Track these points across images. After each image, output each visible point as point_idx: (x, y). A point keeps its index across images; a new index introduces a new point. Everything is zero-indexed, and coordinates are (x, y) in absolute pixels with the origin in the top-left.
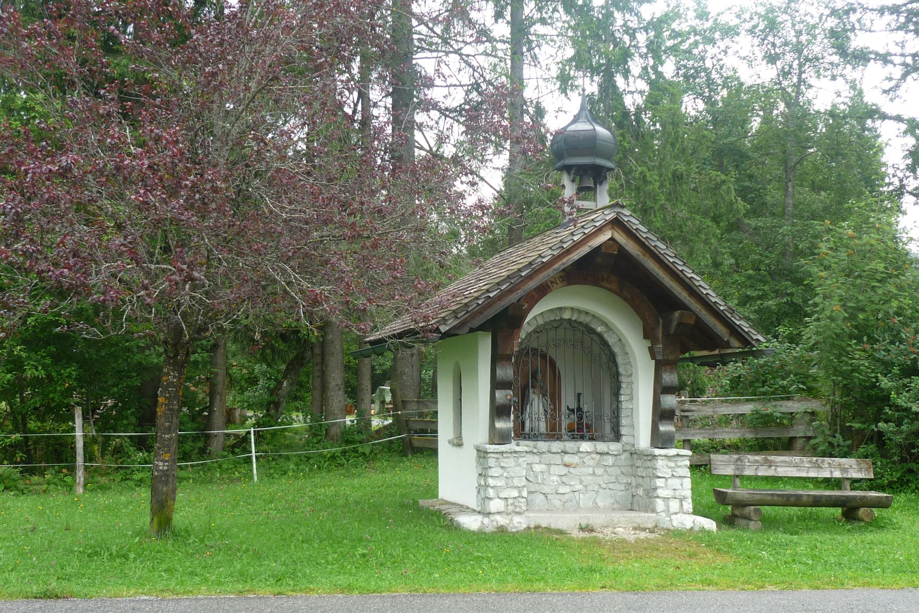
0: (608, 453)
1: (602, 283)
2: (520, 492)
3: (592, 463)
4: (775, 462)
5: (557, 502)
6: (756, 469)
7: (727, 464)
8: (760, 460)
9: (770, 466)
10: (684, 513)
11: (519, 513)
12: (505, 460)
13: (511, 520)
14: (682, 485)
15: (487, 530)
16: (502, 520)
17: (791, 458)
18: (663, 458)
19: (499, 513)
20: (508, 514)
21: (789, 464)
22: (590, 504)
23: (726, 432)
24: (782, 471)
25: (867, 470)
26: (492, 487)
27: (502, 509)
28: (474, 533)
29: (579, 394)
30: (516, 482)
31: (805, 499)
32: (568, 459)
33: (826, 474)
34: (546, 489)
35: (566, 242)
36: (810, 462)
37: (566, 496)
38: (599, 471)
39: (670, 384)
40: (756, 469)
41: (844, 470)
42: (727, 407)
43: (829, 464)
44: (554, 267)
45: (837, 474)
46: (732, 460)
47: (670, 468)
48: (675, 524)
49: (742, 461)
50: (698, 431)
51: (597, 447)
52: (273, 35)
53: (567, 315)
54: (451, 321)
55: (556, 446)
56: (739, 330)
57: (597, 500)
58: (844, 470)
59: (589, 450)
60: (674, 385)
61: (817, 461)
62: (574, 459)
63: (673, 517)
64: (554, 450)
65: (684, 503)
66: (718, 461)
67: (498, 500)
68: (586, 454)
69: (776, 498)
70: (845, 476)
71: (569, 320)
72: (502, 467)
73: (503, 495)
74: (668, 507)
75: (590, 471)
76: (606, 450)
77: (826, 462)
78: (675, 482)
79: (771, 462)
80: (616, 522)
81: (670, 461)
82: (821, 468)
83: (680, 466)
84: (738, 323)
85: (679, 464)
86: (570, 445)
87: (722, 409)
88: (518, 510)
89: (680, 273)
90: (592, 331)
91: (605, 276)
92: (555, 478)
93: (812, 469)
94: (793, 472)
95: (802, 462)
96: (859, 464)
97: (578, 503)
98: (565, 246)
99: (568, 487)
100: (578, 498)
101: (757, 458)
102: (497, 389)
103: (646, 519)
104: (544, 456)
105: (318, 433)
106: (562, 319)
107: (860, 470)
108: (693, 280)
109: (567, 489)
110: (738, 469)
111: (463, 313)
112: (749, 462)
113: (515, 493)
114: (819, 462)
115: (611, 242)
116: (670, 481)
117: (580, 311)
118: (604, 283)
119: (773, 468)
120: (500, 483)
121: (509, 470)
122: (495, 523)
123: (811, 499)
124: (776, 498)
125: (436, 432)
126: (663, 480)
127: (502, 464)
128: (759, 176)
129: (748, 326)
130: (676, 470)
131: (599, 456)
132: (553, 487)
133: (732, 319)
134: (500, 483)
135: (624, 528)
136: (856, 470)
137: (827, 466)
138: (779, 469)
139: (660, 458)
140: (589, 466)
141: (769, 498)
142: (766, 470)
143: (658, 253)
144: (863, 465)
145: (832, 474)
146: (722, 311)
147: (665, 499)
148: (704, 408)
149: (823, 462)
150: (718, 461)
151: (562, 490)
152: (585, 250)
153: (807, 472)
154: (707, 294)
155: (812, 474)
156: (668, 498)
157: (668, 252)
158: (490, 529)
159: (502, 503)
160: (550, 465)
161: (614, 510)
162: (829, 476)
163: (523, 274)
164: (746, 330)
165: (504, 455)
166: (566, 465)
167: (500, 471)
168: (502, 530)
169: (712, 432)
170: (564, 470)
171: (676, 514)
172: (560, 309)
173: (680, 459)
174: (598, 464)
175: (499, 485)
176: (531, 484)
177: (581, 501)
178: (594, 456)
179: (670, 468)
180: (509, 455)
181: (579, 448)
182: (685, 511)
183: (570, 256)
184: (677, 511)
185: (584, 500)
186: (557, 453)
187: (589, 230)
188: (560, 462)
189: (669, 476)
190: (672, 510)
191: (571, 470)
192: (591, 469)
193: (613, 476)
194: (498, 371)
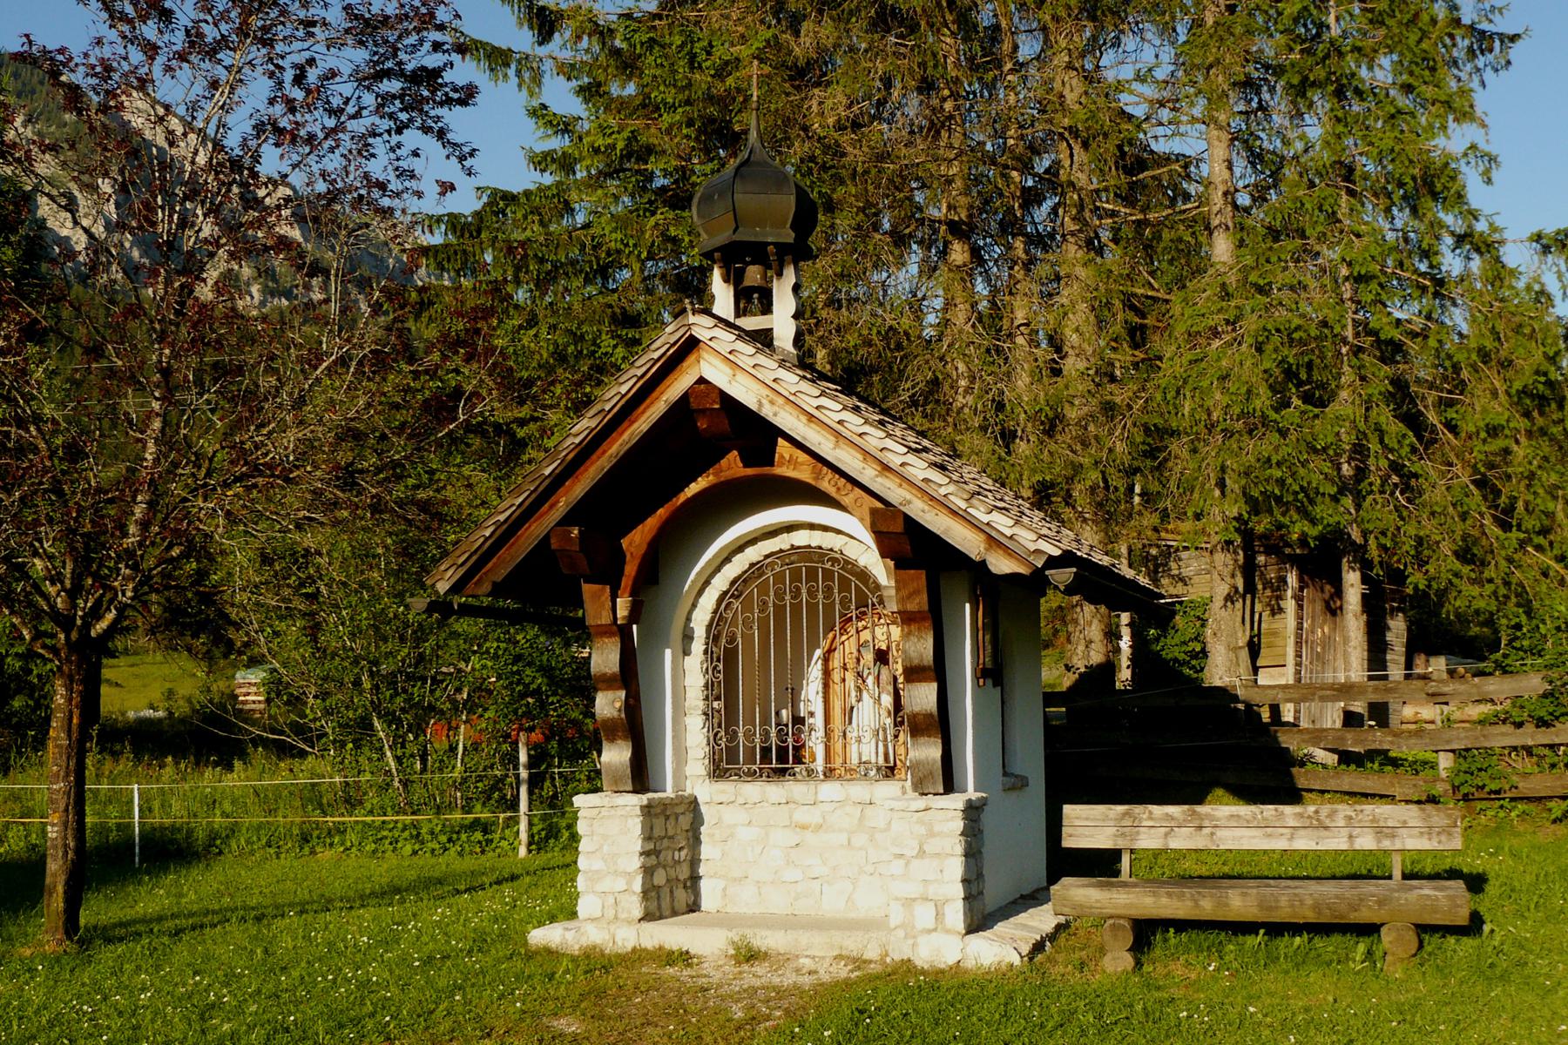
6: (1166, 835)
8: (1176, 815)
19: (593, 920)
32: (802, 815)
36: (1301, 815)
39: (916, 662)
41: (1380, 831)
43: (1350, 818)
44: (610, 452)
45: (1366, 842)
52: (1254, 409)
54: (450, 573)
56: (994, 534)
58: (1380, 831)
60: (926, 663)
61: (1317, 812)
63: (922, 940)
73: (600, 887)
77: (1341, 815)
82: (1326, 828)
93: (1302, 832)
102: (1420, 651)
107: (1429, 831)
111: (466, 555)
120: (597, 864)
126: (902, 862)
128: (1027, 512)
131: (860, 808)
137: (1342, 823)
138: (1220, 833)
142: (1190, 837)
145: (1352, 843)
153: (1291, 838)
156: (914, 900)
162: (1344, 847)
163: (547, 472)
164: (1008, 532)
171: (929, 931)
183: (635, 426)
184: (931, 925)
187: (644, 369)
190: (920, 925)
194: (96, 786)
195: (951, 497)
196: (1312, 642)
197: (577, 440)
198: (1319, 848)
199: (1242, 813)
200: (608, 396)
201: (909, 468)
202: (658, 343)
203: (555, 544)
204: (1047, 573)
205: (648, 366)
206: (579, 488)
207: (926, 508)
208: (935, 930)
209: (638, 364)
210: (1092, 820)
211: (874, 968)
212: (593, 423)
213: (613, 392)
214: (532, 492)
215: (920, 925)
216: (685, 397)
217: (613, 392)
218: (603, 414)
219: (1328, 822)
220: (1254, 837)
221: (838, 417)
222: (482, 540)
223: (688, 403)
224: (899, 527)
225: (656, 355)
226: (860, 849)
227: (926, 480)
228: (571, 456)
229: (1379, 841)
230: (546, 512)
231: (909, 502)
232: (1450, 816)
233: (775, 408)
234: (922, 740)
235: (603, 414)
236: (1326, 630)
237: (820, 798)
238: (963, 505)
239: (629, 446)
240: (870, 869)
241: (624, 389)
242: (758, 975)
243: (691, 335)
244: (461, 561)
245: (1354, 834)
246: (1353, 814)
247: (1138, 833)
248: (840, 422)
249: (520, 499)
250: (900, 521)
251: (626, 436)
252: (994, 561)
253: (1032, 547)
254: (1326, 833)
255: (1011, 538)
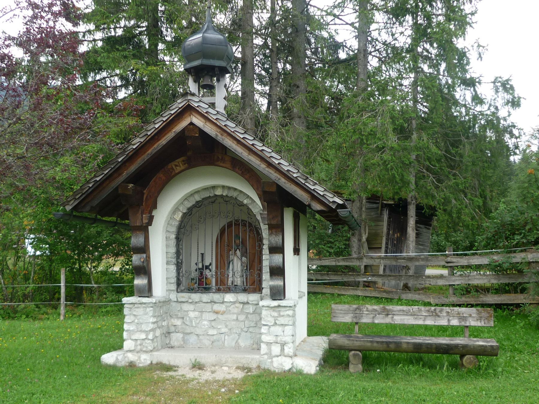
0: (248, 303)
1: (217, 163)
2: (147, 335)
3: (236, 310)
4: (393, 311)
5: (207, 342)
6: (373, 318)
7: (346, 313)
9: (388, 315)
10: (285, 356)
11: (146, 352)
12: (137, 310)
13: (140, 357)
14: (283, 331)
15: (119, 365)
16: (131, 357)
17: (409, 307)
18: (267, 308)
20: (138, 352)
21: (407, 313)
22: (233, 344)
23: (477, 279)
24: (398, 319)
25: (488, 319)
26: (127, 331)
27: (133, 348)
28: (110, 366)
29: (202, 254)
30: (144, 327)
31: (404, 346)
32: (216, 307)
33: (443, 322)
34: (198, 331)
35: (150, 130)
36: (428, 311)
37: (215, 338)
38: (242, 317)
39: (274, 245)
40: (373, 318)
41: (462, 318)
42: (478, 258)
43: (448, 312)
44: (148, 152)
45: (455, 322)
46: (351, 309)
47: (273, 317)
48: (275, 364)
49: (360, 310)
50: (457, 278)
51: (239, 298)
53: (219, 192)
54: (72, 202)
55: (206, 297)
56: (315, 194)
57: (239, 341)
58: (462, 318)
59: (232, 301)
60: (278, 245)
61: (435, 310)
62: (222, 308)
63: (275, 359)
64: (205, 300)
65: (285, 347)
66: (338, 310)
67: (130, 341)
68: (231, 304)
69: (375, 344)
70: (463, 323)
71: (222, 196)
72: (135, 315)
73: (134, 337)
74: (270, 349)
75: (235, 317)
76: (246, 300)
78: (277, 330)
79: (388, 311)
80: (224, 361)
81: (274, 311)
82: (439, 316)
83: (283, 316)
84: (312, 188)
85: (282, 314)
86: (217, 297)
87: (474, 260)
88: (144, 349)
89: (252, 147)
90: (242, 205)
91: (220, 157)
92: (205, 323)
93: (429, 318)
94: (409, 320)
95: (420, 310)
96: (479, 313)
97: (224, 343)
98: (149, 133)
99: (215, 330)
100: (223, 339)
101: (375, 307)
103: (250, 360)
104: (197, 305)
105: (484, 274)
106: (216, 196)
107: (480, 319)
108: (264, 152)
109: (214, 332)
110: (356, 317)
111: (80, 195)
112: (367, 310)
113: (143, 336)
114: (437, 311)
115: (191, 126)
116: (272, 329)
117: (229, 188)
118: (219, 163)
119: (390, 316)
120: (132, 328)
121: (139, 317)
122: (126, 359)
123: (411, 347)
124: (375, 344)
125: (309, 280)
126: (267, 327)
127: (135, 313)
129: (323, 190)
130: (279, 319)
131: (241, 305)
132: (204, 330)
133: (307, 184)
134: (132, 328)
135: (229, 367)
136: (475, 319)
137: (445, 314)
138: (395, 317)
139: (264, 308)
140: (234, 313)
141: (369, 344)
142: (383, 318)
143: (230, 132)
144: (484, 314)
146: (296, 177)
147: (269, 344)
148: (461, 260)
149: (441, 311)
150: (338, 310)
151: (211, 332)
152: (170, 135)
153: (424, 320)
154: (279, 164)
155: (429, 322)
156: (271, 343)
157: (237, 129)
158: (123, 363)
159: (133, 343)
160: (202, 312)
161: (253, 349)
162: (446, 324)
163: (120, 160)
164: (322, 193)
165: (136, 306)
166: (217, 313)
167: (132, 318)
168: (132, 365)
169: (467, 278)
170: (213, 316)
171: (278, 356)
172: (214, 187)
173: (283, 309)
174: (242, 312)
175: (131, 329)
176: (187, 327)
177: (226, 341)
178: (237, 305)
179: (273, 317)
180: (140, 306)
181: (224, 298)
182: (286, 354)
183: (160, 142)
184: (279, 354)
185: (229, 341)
186: (207, 303)
187: (167, 118)
188: (211, 310)
189: (272, 324)
190: (274, 354)
191: (220, 316)
192: (235, 315)
193: (253, 322)
195: (299, 178)
196: (393, 239)
197: (134, 147)
198: (436, 324)
199: (405, 309)
200: (149, 129)
201: (281, 165)
202: (174, 107)
203: (120, 191)
204: (338, 210)
205: (168, 116)
206: (133, 168)
207: (287, 182)
208: (280, 356)
209: (164, 115)
210: (343, 311)
211: (255, 372)
212: (142, 140)
213: (152, 127)
214: (112, 168)
215: (274, 354)
216: (184, 130)
217: (152, 127)
218: (147, 136)
219: (439, 314)
220: (409, 319)
221: (251, 143)
222: (88, 188)
223: (184, 132)
224: (274, 189)
225: (172, 112)
226: (242, 321)
227: (288, 171)
228: (131, 154)
229: (460, 322)
230: (116, 178)
231: (279, 179)
232: (489, 313)
233: (223, 137)
234: (274, 278)
235: (147, 136)
236: (398, 235)
237: (225, 300)
238: (303, 182)
239: (156, 151)
240: (246, 329)
241: (157, 126)
242: (206, 376)
243: (189, 104)
244: (77, 197)
245: (450, 319)
246: (450, 311)
247: (362, 316)
248: (253, 145)
249: (107, 171)
250: (275, 186)
251: (155, 146)
252: (314, 205)
253: (331, 200)
254: (439, 318)
255: (323, 196)
